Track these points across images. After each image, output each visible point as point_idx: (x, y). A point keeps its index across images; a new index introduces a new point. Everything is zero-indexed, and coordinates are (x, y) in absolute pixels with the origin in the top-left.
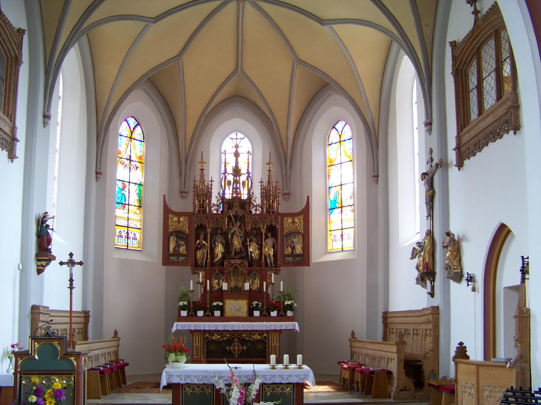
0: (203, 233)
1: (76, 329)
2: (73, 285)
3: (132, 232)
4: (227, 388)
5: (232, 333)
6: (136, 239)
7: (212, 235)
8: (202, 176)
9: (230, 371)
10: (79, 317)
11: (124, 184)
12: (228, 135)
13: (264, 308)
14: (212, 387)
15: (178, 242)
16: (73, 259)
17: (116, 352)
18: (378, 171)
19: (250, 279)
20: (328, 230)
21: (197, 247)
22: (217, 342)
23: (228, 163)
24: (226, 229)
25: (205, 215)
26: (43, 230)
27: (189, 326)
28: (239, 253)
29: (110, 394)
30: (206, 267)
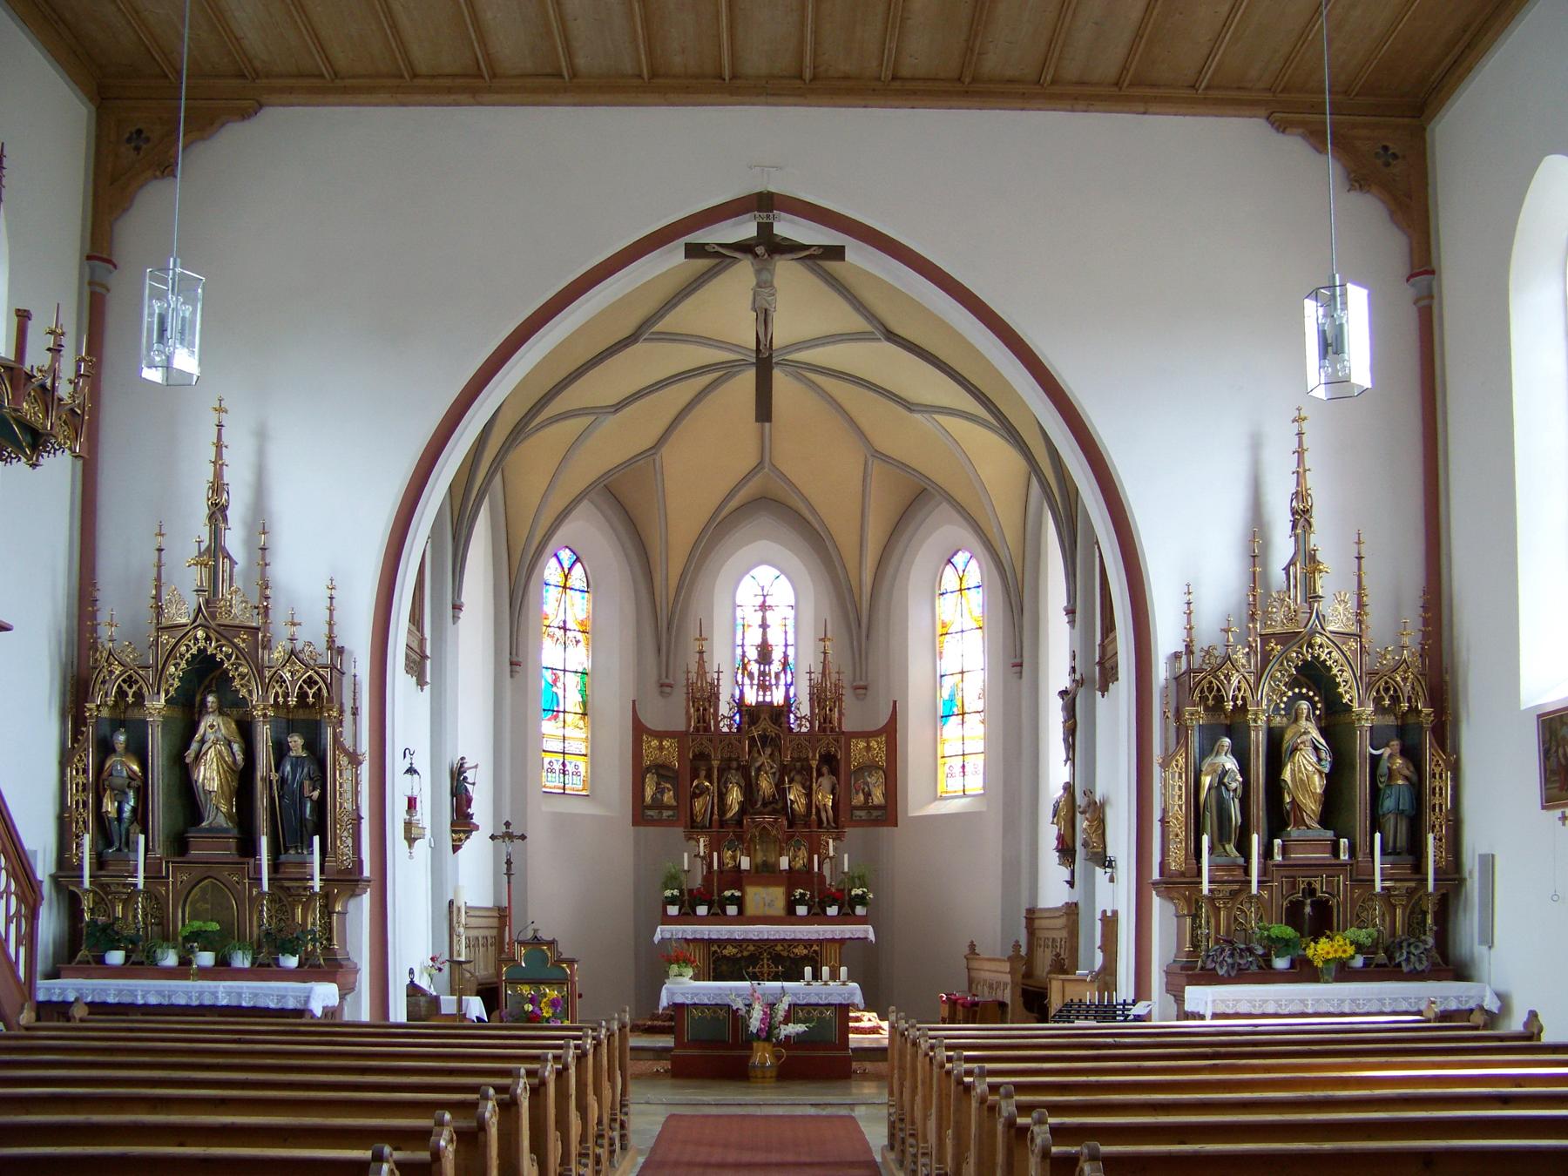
5: (759, 944)
7: (721, 771)
8: (701, 663)
10: (489, 917)
12: (747, 573)
14: (726, 1008)
15: (660, 784)
18: (1022, 656)
20: (939, 755)
21: (694, 793)
23: (749, 626)
28: (771, 803)
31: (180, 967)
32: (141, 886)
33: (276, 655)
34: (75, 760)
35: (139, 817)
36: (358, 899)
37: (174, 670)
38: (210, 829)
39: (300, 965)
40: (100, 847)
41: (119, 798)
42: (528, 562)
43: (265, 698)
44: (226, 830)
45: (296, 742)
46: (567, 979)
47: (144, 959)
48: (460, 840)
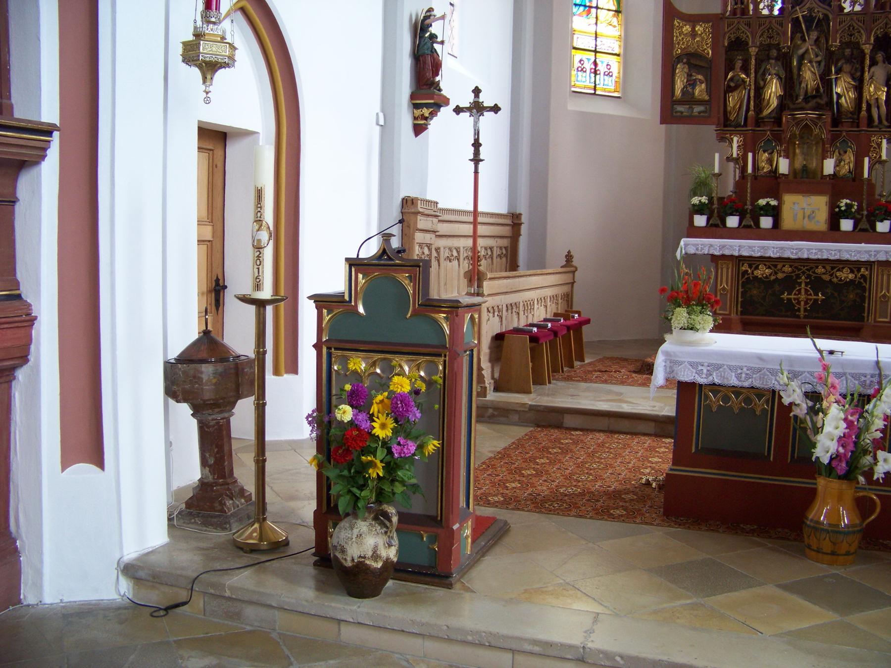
0: (740, 58)
1: (495, 249)
2: (479, 154)
4: (810, 404)
5: (796, 264)
6: (611, 74)
9: (820, 360)
13: (862, 215)
15: (691, 75)
16: (481, 100)
17: (568, 295)
19: (834, 152)
21: (729, 86)
24: (788, 47)
25: (746, 20)
26: (424, 45)
27: (709, 247)
28: (814, 97)
29: (550, 383)
30: (746, 127)
36: (34, 171)
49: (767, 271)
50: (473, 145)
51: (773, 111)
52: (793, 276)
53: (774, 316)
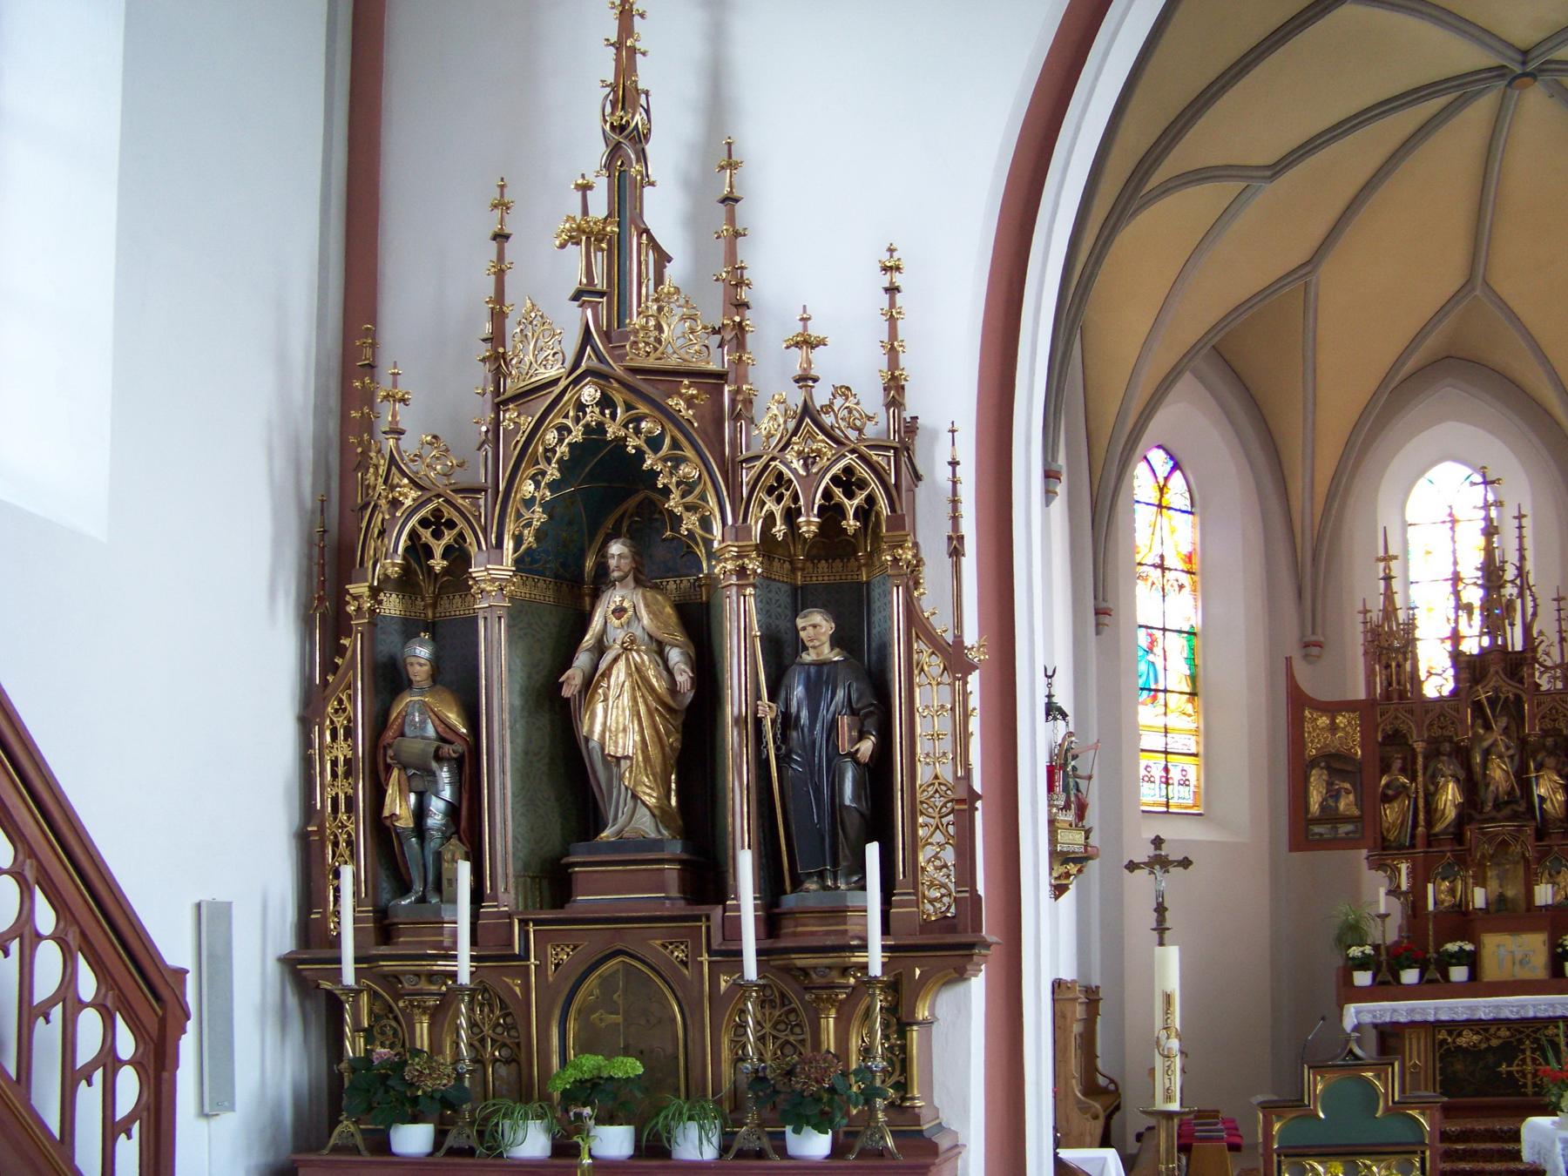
3: (1177, 766)
5: (1515, 1026)
8: (1389, 595)
11: (1150, 635)
22: (1471, 1053)
28: (1507, 803)
31: (558, 1162)
32: (464, 978)
33: (765, 425)
34: (330, 710)
35: (463, 824)
36: (960, 988)
37: (532, 488)
38: (621, 844)
39: (837, 1150)
40: (385, 896)
41: (418, 784)
42: (1119, 454)
43: (741, 531)
44: (656, 845)
45: (817, 628)
46: (1423, 1143)
47: (474, 1142)
48: (1068, 875)
49: (1475, 1037)
50: (1155, 910)
51: (1449, 825)
52: (1512, 1042)
53: (1485, 1095)
